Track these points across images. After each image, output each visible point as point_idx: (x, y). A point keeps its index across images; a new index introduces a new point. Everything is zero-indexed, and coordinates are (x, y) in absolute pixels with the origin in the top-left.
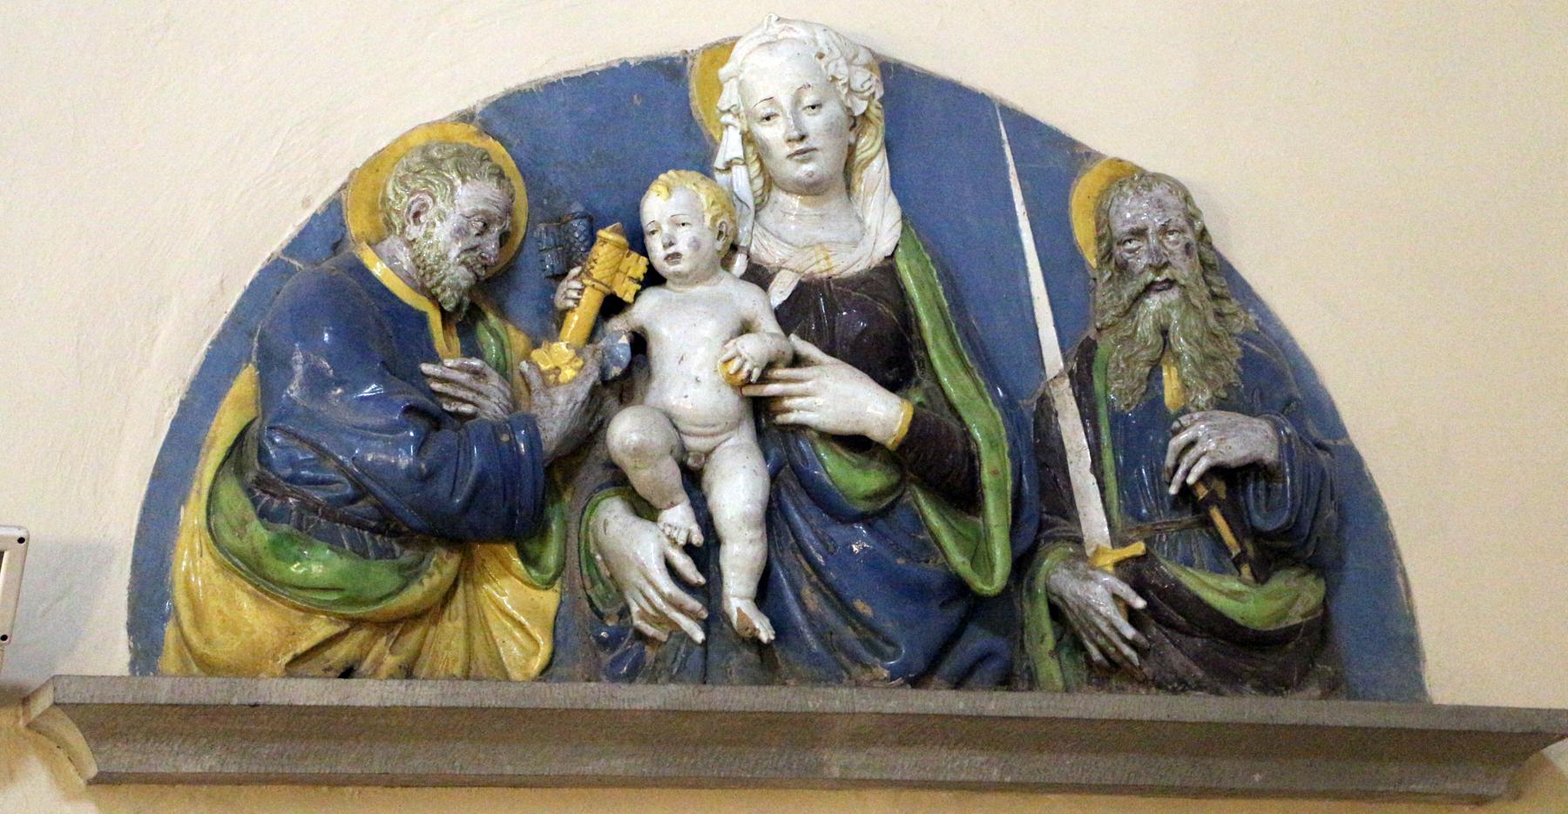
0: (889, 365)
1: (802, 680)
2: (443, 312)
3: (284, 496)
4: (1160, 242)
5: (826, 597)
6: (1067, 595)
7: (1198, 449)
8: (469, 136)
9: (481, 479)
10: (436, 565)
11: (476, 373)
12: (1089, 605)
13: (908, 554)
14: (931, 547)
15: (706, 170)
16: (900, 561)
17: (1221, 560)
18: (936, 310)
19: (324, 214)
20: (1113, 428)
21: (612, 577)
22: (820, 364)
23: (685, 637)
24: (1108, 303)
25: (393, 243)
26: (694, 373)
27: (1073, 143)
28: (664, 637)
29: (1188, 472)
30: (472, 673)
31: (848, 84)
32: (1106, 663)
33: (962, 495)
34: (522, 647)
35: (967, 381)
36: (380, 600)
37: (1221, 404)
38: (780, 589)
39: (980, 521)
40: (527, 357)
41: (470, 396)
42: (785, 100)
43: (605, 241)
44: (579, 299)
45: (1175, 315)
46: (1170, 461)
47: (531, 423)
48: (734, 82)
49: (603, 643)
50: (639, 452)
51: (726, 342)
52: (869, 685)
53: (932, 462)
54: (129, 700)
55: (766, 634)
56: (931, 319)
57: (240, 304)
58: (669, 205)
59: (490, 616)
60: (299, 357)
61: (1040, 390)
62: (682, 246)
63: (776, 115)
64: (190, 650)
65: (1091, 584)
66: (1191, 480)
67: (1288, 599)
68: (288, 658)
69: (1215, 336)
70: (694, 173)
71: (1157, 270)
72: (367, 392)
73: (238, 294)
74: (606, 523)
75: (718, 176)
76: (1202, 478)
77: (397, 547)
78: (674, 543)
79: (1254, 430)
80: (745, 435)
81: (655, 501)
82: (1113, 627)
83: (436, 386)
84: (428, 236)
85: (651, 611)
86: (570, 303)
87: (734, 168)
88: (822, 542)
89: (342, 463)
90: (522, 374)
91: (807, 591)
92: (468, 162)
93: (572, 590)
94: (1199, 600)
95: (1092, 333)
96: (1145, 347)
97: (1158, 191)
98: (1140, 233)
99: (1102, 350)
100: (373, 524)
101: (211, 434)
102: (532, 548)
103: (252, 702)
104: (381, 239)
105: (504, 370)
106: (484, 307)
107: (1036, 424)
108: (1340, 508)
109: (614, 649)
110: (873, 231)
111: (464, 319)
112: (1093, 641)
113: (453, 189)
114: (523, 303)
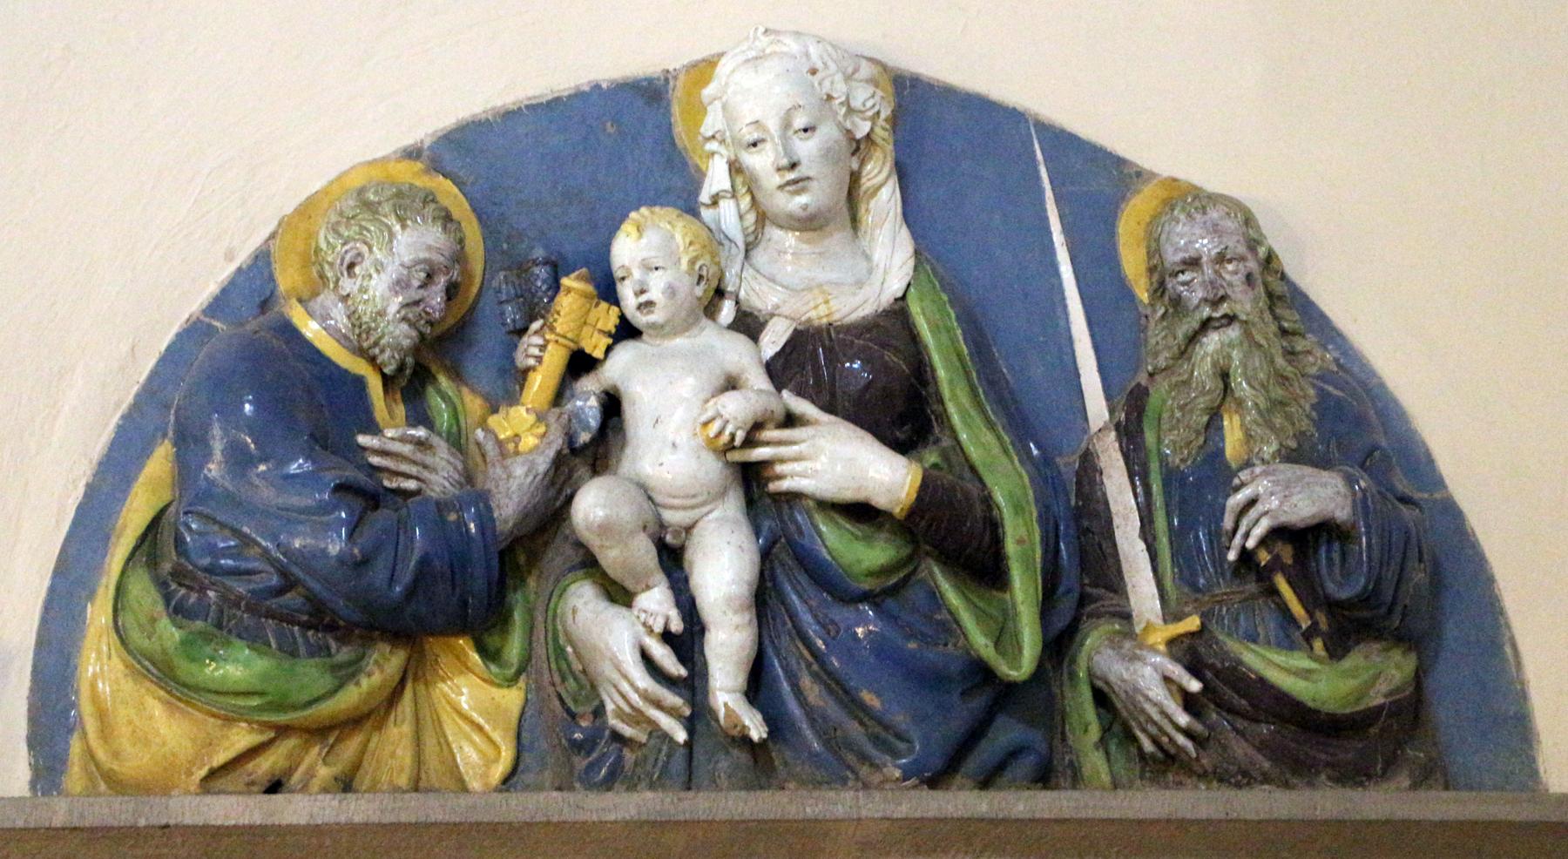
0: (902, 420)
1: (802, 783)
2: (385, 377)
3: (202, 590)
4: (1216, 272)
5: (828, 687)
6: (1112, 678)
7: (1259, 508)
8: (415, 174)
9: (424, 562)
10: (376, 662)
11: (420, 444)
12: (1137, 690)
13: (922, 637)
14: (950, 628)
15: (691, 209)
16: (912, 645)
17: (1289, 635)
18: (955, 359)
19: (250, 268)
20: (1166, 483)
21: (584, 671)
22: (816, 423)
23: (666, 737)
24: (1160, 340)
25: (327, 299)
26: (671, 437)
27: (1120, 162)
28: (643, 738)
29: (1247, 535)
30: (421, 784)
31: (847, 103)
32: (1160, 755)
33: (984, 568)
34: (479, 751)
35: (989, 437)
36: (309, 704)
37: (1292, 456)
38: (776, 679)
39: (1007, 596)
40: (483, 424)
41: (413, 470)
42: (773, 125)
43: (569, 290)
44: (543, 359)
45: (1236, 354)
46: (1228, 523)
47: (482, 500)
48: (718, 104)
49: (577, 747)
50: (605, 529)
51: (707, 401)
52: (880, 787)
53: (949, 530)
54: (20, 824)
55: (756, 729)
56: (947, 369)
57: (154, 374)
58: (646, 250)
59: (444, 717)
60: (216, 431)
61: (1083, 446)
62: (655, 293)
63: (763, 141)
64: (97, 765)
65: (1138, 665)
66: (1251, 544)
67: (1365, 676)
68: (203, 772)
69: (1283, 379)
70: (670, 209)
71: (1216, 303)
72: (293, 468)
73: (150, 364)
74: (574, 611)
75: (706, 214)
76: (1263, 542)
77: (333, 645)
78: (650, 631)
79: (1325, 485)
80: (732, 507)
81: (629, 584)
82: (1163, 713)
83: (375, 460)
84: (363, 290)
85: (627, 709)
86: (531, 362)
87: (722, 203)
88: (824, 626)
89: (266, 551)
90: (478, 444)
91: (806, 682)
92: (407, 203)
93: (539, 688)
94: (1262, 680)
95: (1143, 379)
96: (1203, 393)
97: (1214, 214)
98: (1193, 263)
99: (1154, 401)
100: (305, 618)
101: (121, 522)
102: (492, 641)
103: (164, 822)
104: (315, 294)
105: (457, 441)
106: (434, 369)
107: (1079, 483)
108: (1436, 565)
109: (589, 753)
110: (882, 266)
111: (411, 382)
112: (1144, 730)
113: (392, 235)
114: (480, 365)
